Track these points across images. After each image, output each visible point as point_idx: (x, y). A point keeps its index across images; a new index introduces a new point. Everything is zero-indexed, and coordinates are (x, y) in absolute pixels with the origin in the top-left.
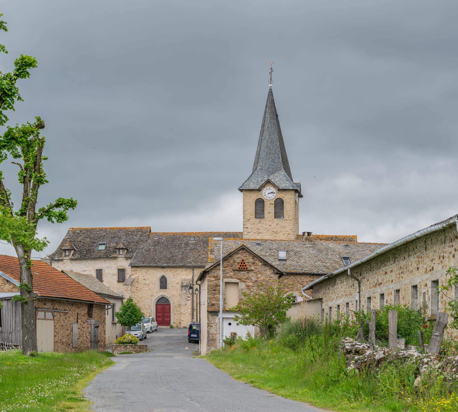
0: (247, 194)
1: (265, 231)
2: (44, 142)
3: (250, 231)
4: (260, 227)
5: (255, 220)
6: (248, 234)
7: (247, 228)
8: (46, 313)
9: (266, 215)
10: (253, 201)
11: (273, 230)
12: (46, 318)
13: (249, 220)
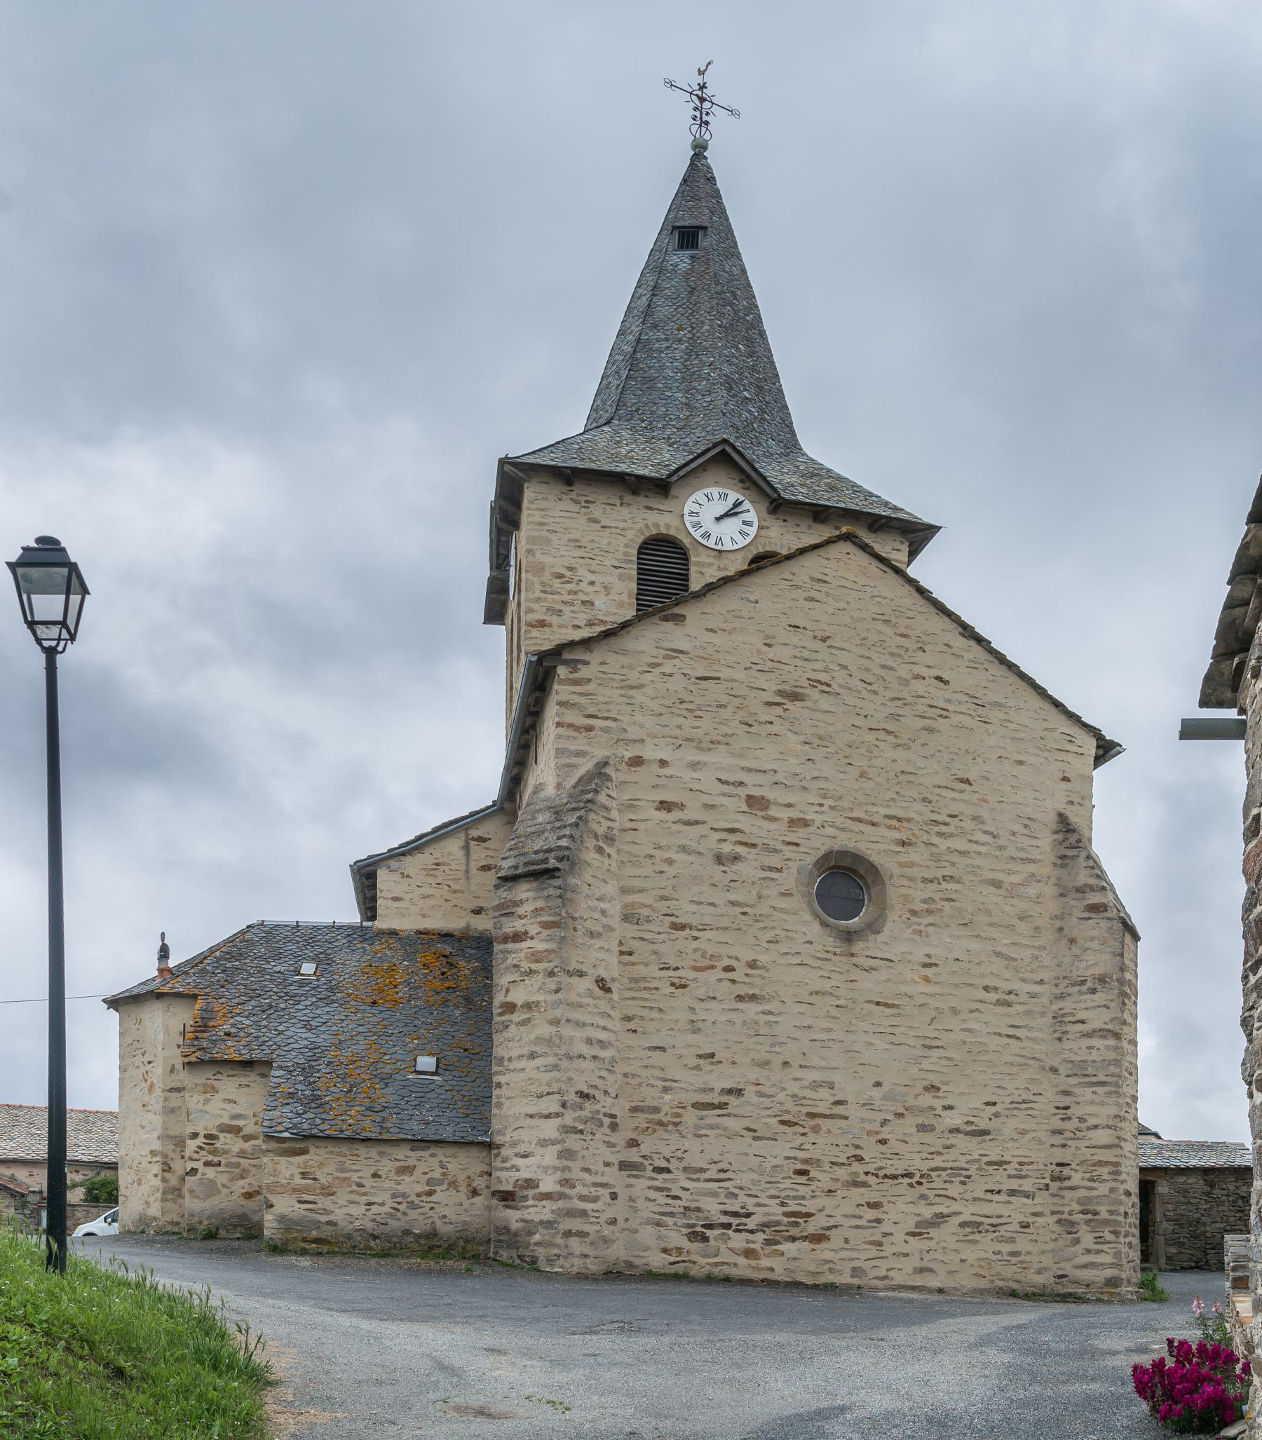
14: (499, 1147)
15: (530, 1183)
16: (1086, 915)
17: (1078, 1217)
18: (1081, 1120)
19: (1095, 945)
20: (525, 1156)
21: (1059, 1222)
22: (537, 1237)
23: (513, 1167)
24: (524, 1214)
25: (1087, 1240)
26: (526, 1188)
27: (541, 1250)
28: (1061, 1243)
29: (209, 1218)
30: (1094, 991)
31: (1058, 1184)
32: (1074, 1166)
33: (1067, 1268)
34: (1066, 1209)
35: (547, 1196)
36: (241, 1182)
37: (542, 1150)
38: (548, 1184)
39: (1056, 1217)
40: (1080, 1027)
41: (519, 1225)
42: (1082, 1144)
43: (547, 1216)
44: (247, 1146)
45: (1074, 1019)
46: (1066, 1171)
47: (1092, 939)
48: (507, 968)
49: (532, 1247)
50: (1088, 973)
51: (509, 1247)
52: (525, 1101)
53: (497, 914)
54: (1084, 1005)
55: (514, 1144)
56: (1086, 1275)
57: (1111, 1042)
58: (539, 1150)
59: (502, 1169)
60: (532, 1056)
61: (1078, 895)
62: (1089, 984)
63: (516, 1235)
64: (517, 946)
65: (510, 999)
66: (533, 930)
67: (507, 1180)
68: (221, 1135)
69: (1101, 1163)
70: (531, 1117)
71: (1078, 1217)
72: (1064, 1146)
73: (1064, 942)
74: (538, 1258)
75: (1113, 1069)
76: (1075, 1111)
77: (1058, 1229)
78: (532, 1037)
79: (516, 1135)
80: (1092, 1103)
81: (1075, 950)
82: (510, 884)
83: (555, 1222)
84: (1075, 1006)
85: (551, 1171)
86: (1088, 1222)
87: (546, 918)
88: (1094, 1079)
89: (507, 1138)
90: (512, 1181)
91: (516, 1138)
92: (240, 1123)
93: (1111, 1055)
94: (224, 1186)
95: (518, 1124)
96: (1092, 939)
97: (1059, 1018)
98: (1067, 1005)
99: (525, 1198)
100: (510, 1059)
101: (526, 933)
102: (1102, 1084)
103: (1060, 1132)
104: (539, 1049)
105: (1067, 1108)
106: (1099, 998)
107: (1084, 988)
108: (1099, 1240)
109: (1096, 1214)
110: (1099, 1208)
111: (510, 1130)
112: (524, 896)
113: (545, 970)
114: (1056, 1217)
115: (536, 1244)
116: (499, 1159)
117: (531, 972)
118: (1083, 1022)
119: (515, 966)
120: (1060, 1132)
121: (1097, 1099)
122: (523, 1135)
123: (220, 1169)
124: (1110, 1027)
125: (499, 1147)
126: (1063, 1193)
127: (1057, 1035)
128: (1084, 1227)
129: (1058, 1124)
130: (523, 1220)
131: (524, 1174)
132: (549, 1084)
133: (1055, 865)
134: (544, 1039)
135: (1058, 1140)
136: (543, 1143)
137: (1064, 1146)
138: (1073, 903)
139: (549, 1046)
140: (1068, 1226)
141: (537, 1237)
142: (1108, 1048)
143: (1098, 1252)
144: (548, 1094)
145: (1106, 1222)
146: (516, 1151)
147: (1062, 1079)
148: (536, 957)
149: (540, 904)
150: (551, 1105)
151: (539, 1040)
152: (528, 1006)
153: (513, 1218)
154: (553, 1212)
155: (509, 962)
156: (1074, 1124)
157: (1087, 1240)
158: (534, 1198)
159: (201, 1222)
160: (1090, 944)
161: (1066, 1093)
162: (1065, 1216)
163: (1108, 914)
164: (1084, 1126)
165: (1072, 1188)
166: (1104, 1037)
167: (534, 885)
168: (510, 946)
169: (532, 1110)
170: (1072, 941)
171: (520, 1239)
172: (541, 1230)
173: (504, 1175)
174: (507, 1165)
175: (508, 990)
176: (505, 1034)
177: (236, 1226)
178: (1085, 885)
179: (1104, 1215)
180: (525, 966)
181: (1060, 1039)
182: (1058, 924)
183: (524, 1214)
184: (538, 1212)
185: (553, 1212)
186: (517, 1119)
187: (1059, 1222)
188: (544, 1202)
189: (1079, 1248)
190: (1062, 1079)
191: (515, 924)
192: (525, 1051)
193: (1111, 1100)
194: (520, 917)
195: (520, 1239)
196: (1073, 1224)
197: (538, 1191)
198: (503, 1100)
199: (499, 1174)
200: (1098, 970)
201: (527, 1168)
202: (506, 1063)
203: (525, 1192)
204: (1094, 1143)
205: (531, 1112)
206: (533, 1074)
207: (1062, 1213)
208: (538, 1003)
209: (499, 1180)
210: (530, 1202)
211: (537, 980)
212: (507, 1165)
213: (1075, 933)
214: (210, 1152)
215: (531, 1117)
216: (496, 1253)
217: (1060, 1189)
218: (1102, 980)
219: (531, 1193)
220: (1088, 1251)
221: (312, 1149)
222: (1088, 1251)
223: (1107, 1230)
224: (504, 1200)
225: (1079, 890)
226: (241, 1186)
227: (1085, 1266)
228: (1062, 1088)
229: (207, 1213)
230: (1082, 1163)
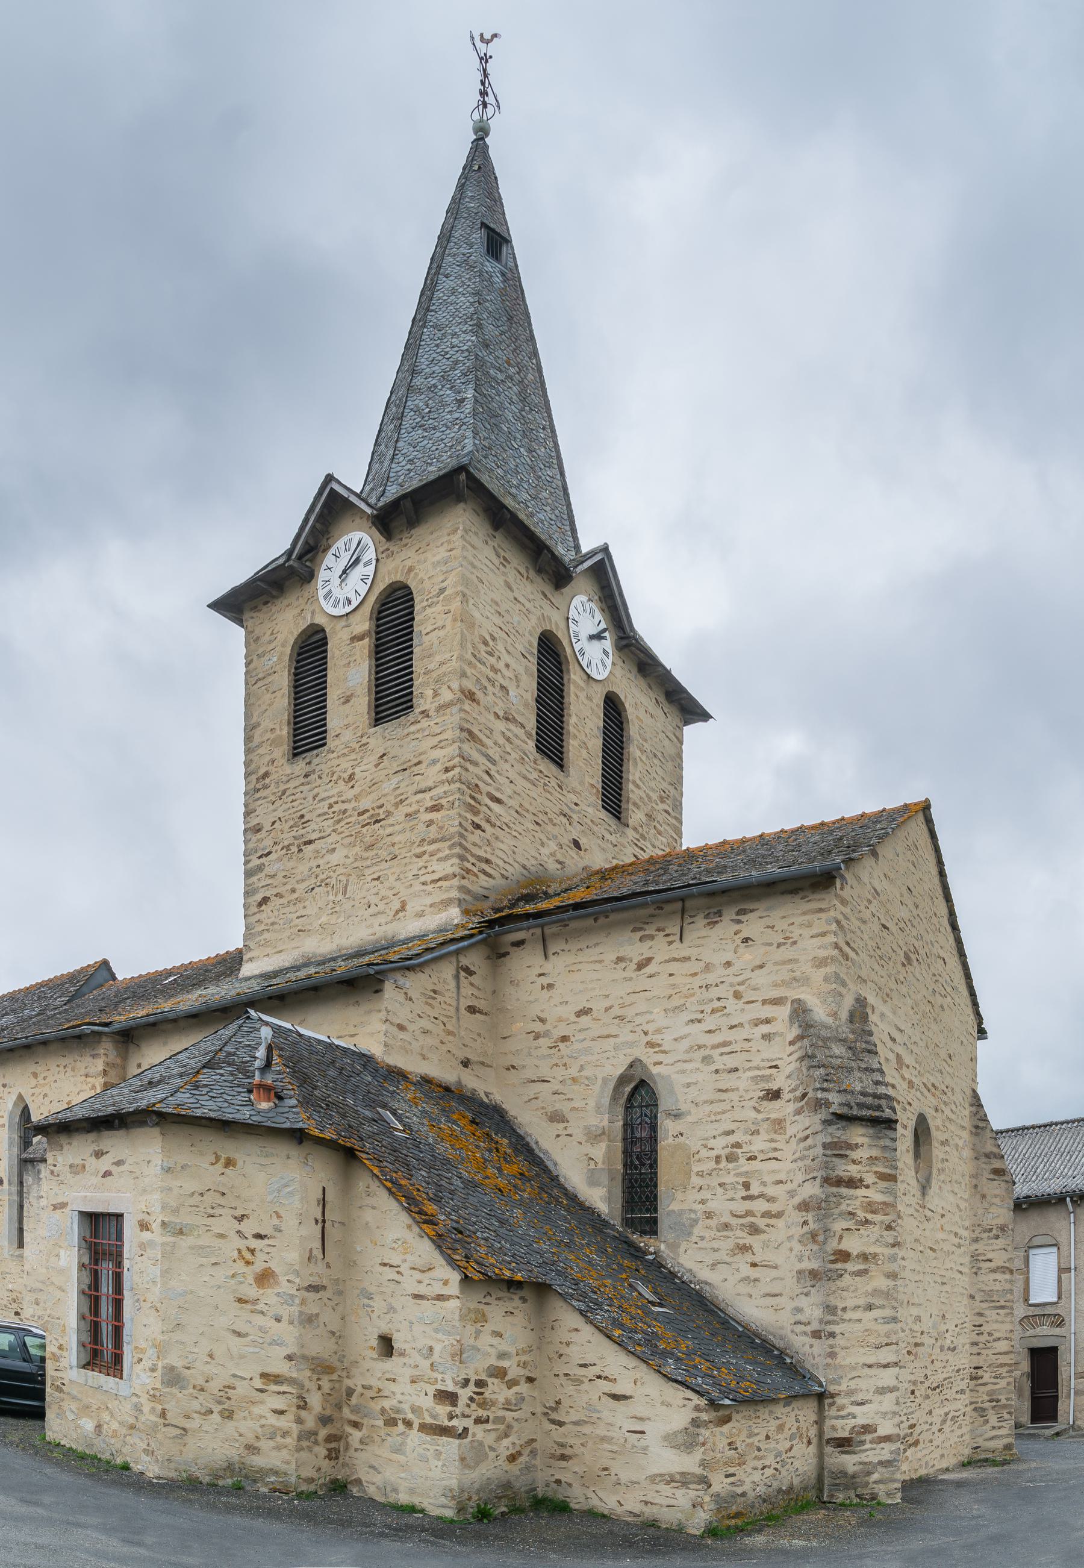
14: (832, 1396)
15: (867, 1429)
16: (992, 1176)
17: (987, 1405)
18: (990, 1334)
19: (997, 1201)
20: (862, 1404)
21: (975, 1409)
22: (876, 1476)
23: (849, 1414)
24: (862, 1457)
25: (993, 1420)
26: (863, 1433)
27: (881, 1486)
28: (976, 1424)
29: (478, 1492)
30: (997, 1237)
31: (974, 1382)
32: (985, 1368)
33: (980, 1442)
34: (980, 1400)
35: (887, 1439)
36: (506, 1442)
37: (881, 1397)
38: (885, 1428)
39: (973, 1406)
40: (988, 1264)
41: (857, 1468)
42: (990, 1352)
43: (886, 1455)
44: (510, 1394)
45: (985, 1258)
46: (980, 1372)
47: (996, 1196)
48: (840, 1215)
49: (870, 1486)
50: (994, 1222)
51: (847, 1488)
52: (862, 1351)
53: (829, 1152)
54: (991, 1248)
55: (851, 1392)
56: (992, 1444)
57: (1007, 1276)
58: (878, 1398)
59: (837, 1418)
60: (870, 1307)
61: (987, 1160)
62: (994, 1232)
63: (853, 1477)
64: (852, 1192)
65: (845, 1246)
66: (869, 1179)
67: (842, 1428)
68: (490, 1381)
69: (1002, 1365)
70: (870, 1366)
71: (987, 1405)
72: (979, 1354)
73: (978, 1196)
74: (877, 1494)
75: (1009, 1296)
76: (986, 1328)
77: (975, 1414)
78: (869, 1288)
79: (853, 1385)
80: (997, 1321)
81: (986, 1205)
82: (844, 1123)
83: (895, 1460)
84: (986, 1248)
85: (890, 1416)
86: (993, 1407)
87: (881, 1169)
88: (998, 1304)
89: (843, 1387)
90: (848, 1429)
91: (853, 1387)
92: (505, 1364)
93: (1008, 1286)
94: (492, 1449)
95: (854, 1374)
96: (996, 1196)
97: (975, 1257)
98: (980, 1247)
99: (863, 1442)
100: (844, 1309)
101: (861, 1180)
102: (1002, 1307)
103: (976, 1344)
104: (877, 1302)
105: (980, 1326)
106: (1000, 1243)
107: (991, 1235)
108: (1000, 1419)
109: (998, 1401)
110: (1000, 1397)
111: (846, 1379)
112: (860, 1140)
113: (882, 1222)
114: (973, 1406)
115: (875, 1482)
116: (834, 1408)
117: (867, 1222)
118: (990, 1261)
119: (851, 1214)
120: (976, 1344)
121: (1000, 1318)
122: (862, 1384)
123: (489, 1426)
124: (1007, 1265)
125: (832, 1396)
126: (978, 1388)
127: (974, 1270)
128: (991, 1412)
129: (976, 1339)
130: (861, 1463)
131: (861, 1421)
132: (887, 1335)
133: (971, 1133)
134: (882, 1292)
135: (975, 1350)
136: (881, 1391)
137: (979, 1354)
138: (984, 1166)
139: (887, 1299)
140: (980, 1411)
141: (876, 1476)
142: (1006, 1281)
143: (1000, 1428)
144: (887, 1345)
145: (1005, 1406)
146: (853, 1399)
147: (977, 1303)
148: (871, 1207)
149: (875, 1153)
150: (887, 1355)
151: (876, 1292)
152: (864, 1257)
153: (849, 1462)
154: (892, 1452)
155: (843, 1207)
156: (985, 1337)
157: (993, 1420)
158: (871, 1442)
159: (470, 1499)
160: (994, 1200)
161: (980, 1315)
162: (979, 1405)
163: (1005, 1178)
164: (991, 1338)
165: (984, 1384)
166: (1004, 1272)
167: (871, 1131)
168: (844, 1191)
169: (871, 1360)
170: (984, 1196)
171: (858, 1480)
172: (880, 1469)
173: (838, 1423)
174: (842, 1413)
175: (841, 1237)
176: (838, 1283)
177: (500, 1498)
178: (991, 1152)
179: (1004, 1402)
180: (861, 1215)
181: (976, 1273)
182: (974, 1182)
183: (862, 1457)
184: (873, 1453)
185: (892, 1452)
186: (854, 1368)
187: (975, 1409)
188: (883, 1445)
189: (988, 1427)
190: (977, 1303)
191: (849, 1168)
192: (861, 1302)
193: (1008, 1319)
194: (854, 1162)
195: (858, 1480)
196: (984, 1410)
197: (875, 1435)
198: (837, 1350)
199: (834, 1422)
200: (1000, 1221)
201: (863, 1416)
202: (839, 1313)
203: (863, 1438)
204: (997, 1350)
205: (868, 1362)
206: (872, 1326)
207: (977, 1403)
208: (876, 1255)
209: (834, 1428)
210: (868, 1446)
211: (875, 1231)
212: (842, 1413)
213: (985, 1191)
214: (480, 1405)
215: (870, 1366)
216: (832, 1496)
217: (976, 1385)
218: (1002, 1228)
219: (868, 1437)
220: (994, 1428)
221: (735, 1416)
222: (994, 1428)
223: (1005, 1412)
224: (839, 1446)
225: (987, 1156)
226: (506, 1446)
227: (992, 1438)
228: (977, 1310)
229: (476, 1486)
230: (990, 1366)
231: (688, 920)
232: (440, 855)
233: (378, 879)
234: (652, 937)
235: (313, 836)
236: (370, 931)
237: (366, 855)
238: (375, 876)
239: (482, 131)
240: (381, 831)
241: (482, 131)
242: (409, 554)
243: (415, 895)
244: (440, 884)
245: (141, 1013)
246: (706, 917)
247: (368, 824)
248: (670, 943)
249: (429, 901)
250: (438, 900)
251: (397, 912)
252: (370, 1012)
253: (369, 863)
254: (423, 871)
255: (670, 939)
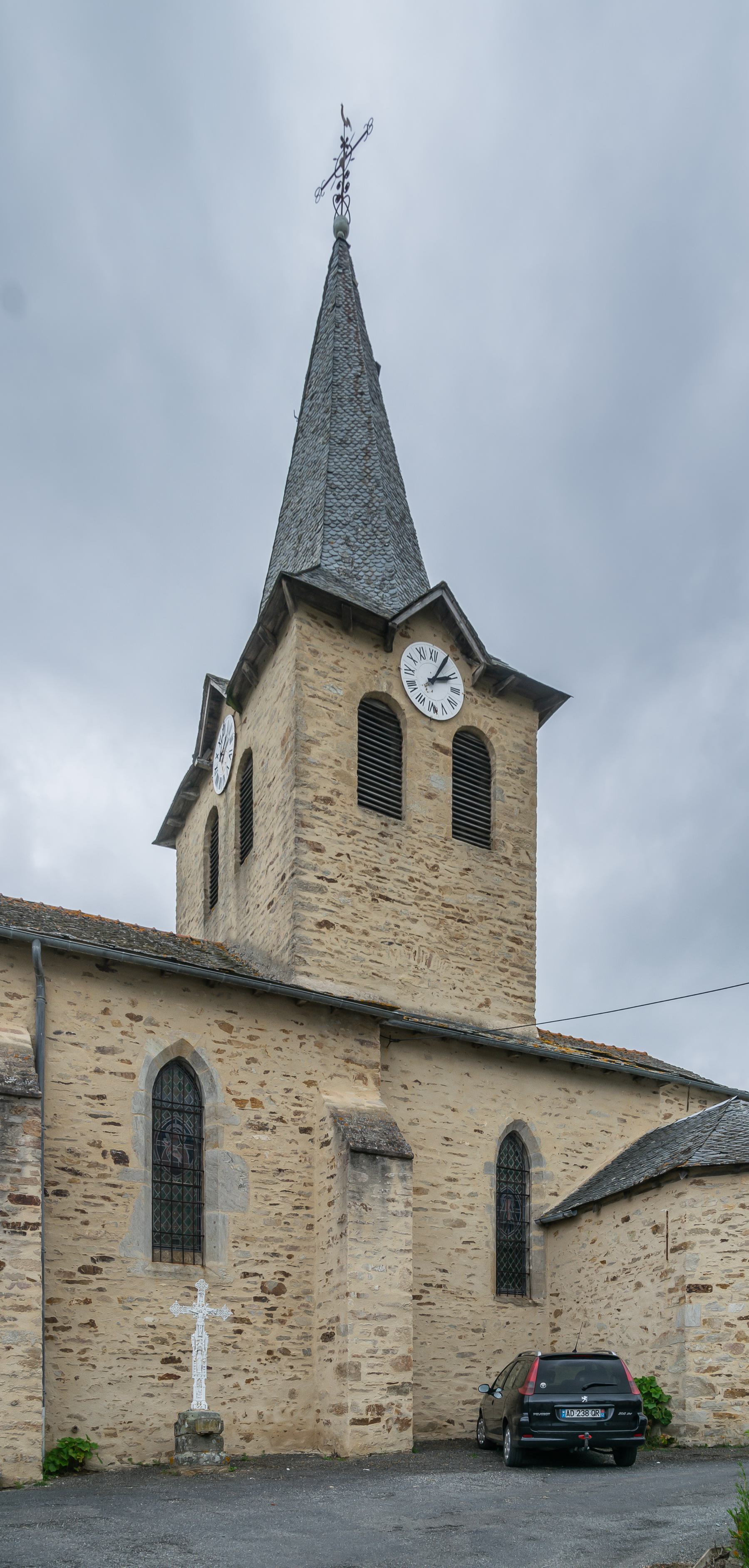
0: (316, 644)
1: (409, 896)
2: (429, 680)
3: (333, 871)
4: (384, 863)
5: (359, 813)
6: (322, 890)
7: (318, 849)
8: (299, 632)
9: (414, 803)
10: (348, 696)
11: (449, 899)
12: (299, 632)
13: (327, 800)
231: (690, 1100)
232: (520, 979)
233: (463, 969)
234: (672, 1102)
235: (391, 896)
236: (456, 1009)
237: (449, 942)
238: (461, 966)
239: (341, 232)
240: (465, 931)
241: (341, 232)
242: (491, 715)
243: (498, 999)
244: (519, 1000)
245: (557, 1048)
246: (699, 1102)
247: (452, 918)
248: (681, 1109)
249: (511, 1009)
250: (519, 1012)
251: (481, 1005)
252: (649, 1105)
253: (453, 951)
254: (505, 984)
255: (681, 1107)
